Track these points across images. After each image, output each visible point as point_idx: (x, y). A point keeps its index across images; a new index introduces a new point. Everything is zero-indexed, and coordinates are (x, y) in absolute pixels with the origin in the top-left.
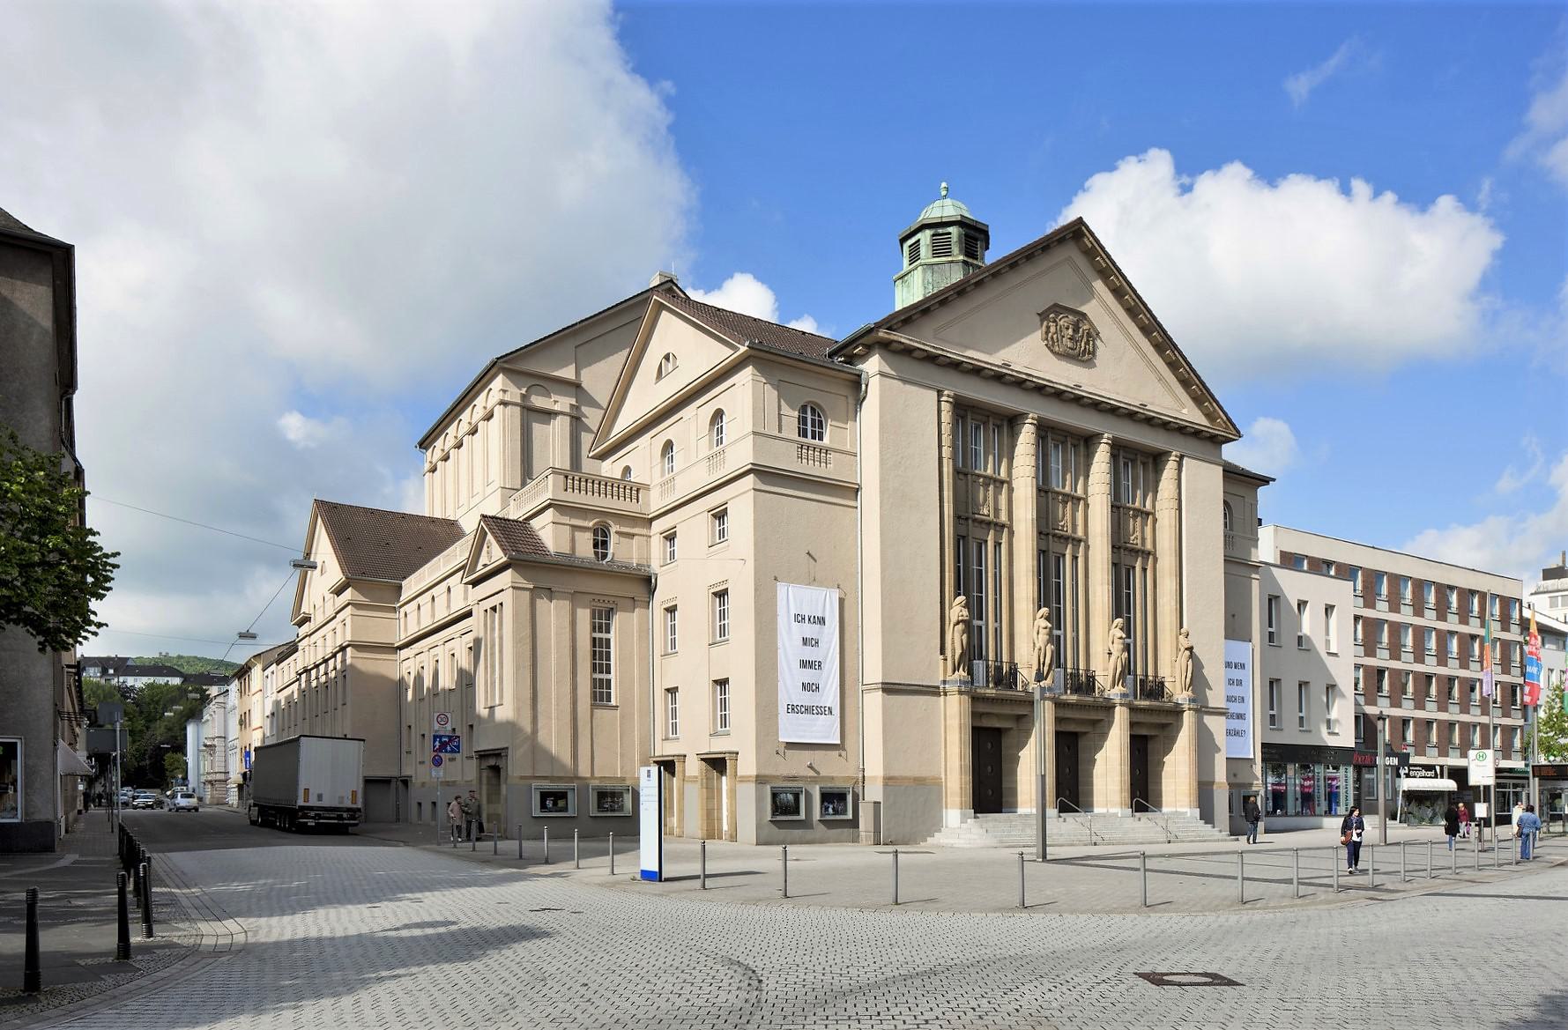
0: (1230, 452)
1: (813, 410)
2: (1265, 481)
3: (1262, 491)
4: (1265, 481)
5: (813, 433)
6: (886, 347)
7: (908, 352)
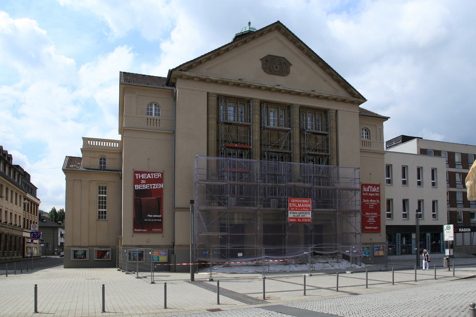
0: (361, 106)
1: (365, 130)
2: (386, 118)
3: (385, 123)
4: (386, 118)
5: (365, 137)
6: (181, 77)
7: (192, 78)
